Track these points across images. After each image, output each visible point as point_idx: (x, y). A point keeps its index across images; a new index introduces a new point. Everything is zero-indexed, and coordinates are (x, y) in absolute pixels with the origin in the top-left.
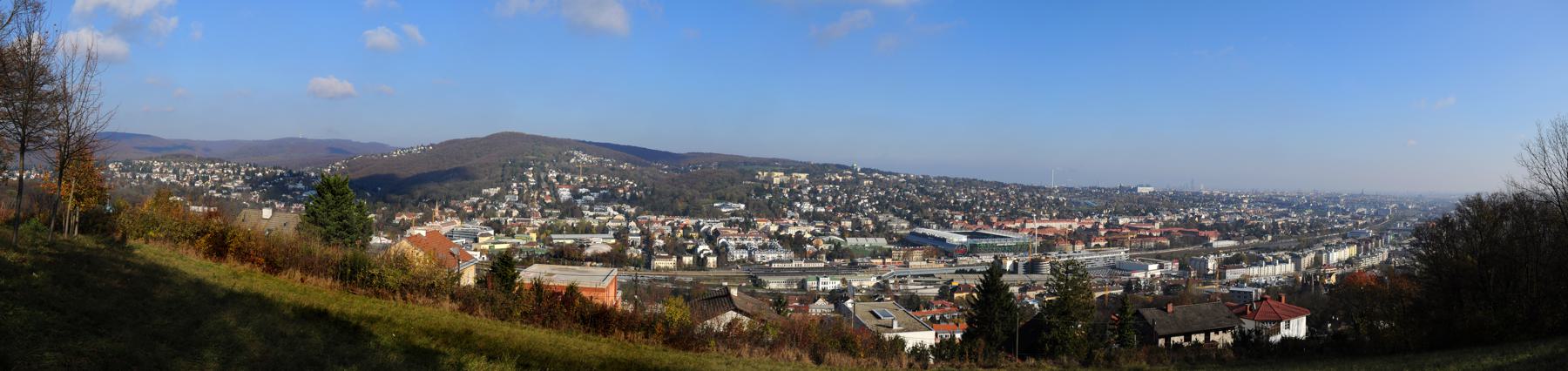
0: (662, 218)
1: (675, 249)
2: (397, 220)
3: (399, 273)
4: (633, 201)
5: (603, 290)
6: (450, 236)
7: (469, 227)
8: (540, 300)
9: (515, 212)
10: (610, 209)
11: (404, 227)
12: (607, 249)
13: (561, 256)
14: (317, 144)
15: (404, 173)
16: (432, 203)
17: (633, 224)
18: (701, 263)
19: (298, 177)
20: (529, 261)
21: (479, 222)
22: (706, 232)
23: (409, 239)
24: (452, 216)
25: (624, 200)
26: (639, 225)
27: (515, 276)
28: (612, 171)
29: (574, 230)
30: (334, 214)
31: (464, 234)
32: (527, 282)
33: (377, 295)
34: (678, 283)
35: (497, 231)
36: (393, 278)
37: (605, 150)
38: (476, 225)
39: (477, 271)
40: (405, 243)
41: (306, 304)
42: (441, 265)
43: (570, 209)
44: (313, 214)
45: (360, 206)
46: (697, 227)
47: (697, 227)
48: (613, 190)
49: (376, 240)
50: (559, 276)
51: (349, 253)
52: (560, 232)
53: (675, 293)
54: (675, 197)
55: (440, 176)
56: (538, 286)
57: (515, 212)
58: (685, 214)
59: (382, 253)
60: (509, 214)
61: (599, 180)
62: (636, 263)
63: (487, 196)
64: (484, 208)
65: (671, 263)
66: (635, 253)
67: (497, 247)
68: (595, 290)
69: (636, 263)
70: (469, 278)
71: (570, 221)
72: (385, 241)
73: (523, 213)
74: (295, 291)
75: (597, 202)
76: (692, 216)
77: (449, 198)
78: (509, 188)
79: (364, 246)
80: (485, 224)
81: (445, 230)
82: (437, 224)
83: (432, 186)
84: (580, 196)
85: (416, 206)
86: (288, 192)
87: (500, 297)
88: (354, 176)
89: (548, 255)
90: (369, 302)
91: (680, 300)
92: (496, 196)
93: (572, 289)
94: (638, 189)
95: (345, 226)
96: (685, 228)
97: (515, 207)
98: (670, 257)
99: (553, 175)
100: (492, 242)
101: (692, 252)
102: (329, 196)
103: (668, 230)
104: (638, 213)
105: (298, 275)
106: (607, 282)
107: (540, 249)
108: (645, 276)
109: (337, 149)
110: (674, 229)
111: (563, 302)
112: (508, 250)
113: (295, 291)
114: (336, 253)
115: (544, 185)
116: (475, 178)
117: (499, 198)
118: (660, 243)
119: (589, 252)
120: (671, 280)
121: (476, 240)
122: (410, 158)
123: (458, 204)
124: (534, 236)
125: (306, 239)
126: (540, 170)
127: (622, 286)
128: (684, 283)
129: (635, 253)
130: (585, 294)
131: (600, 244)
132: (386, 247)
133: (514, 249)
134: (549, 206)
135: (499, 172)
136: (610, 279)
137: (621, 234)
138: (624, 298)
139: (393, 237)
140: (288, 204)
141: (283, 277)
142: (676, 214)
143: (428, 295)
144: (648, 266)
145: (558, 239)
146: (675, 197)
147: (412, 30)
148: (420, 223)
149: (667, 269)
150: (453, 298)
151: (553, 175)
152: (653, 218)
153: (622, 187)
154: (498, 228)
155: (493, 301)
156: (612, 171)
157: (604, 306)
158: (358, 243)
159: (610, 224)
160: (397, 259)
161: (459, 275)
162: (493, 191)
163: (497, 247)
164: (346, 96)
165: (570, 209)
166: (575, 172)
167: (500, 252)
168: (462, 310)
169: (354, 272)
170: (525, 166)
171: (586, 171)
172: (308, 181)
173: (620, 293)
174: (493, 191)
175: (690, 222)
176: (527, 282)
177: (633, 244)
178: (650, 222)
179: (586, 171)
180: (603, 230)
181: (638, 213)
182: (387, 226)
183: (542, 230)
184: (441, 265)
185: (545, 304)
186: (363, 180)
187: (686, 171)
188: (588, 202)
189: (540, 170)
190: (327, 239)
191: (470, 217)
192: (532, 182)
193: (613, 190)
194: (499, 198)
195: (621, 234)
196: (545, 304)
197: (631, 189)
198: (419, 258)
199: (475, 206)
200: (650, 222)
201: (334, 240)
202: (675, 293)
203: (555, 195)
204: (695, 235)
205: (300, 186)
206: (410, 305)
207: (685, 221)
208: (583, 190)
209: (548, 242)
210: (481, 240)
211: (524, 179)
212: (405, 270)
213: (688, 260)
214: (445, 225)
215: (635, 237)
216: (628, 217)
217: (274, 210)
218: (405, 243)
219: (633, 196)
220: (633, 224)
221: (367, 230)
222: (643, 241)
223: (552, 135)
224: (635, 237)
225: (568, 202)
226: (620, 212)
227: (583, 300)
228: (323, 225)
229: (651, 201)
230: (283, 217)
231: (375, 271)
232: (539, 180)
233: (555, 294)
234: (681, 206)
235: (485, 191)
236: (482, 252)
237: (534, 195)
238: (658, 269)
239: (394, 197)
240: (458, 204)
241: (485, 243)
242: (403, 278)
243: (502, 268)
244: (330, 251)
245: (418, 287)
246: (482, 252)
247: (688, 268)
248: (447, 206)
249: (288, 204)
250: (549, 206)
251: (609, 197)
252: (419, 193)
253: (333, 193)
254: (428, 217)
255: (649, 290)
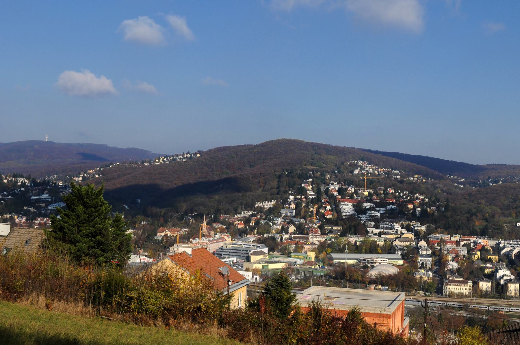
0: (457, 238)
1: (471, 273)
2: (159, 236)
3: (161, 295)
4: (423, 218)
5: (388, 317)
6: (219, 254)
7: (241, 244)
8: (318, 326)
9: (292, 229)
10: (397, 227)
11: (166, 245)
12: (393, 271)
13: (342, 277)
14: (66, 149)
15: (166, 184)
16: (199, 217)
17: (423, 243)
18: (500, 290)
19: (41, 186)
20: (306, 282)
21: (251, 238)
22: (508, 255)
23: (172, 258)
24: (222, 231)
25: (413, 217)
26: (430, 245)
27: (290, 299)
28: (400, 185)
29: (356, 249)
30: (86, 229)
31: (234, 252)
32: (304, 305)
33: (136, 320)
34: (473, 311)
35: (272, 249)
36: (154, 301)
37: (393, 160)
38: (249, 241)
39: (249, 293)
40: (168, 263)
41: (52, 333)
42: (208, 286)
43: (352, 225)
44: (61, 229)
45: (117, 221)
46: (497, 249)
47: (497, 249)
48: (402, 205)
49: (135, 259)
50: (339, 300)
51: (104, 273)
52: (342, 251)
53: (471, 322)
54: (471, 214)
55: (208, 188)
56: (316, 311)
57: (292, 229)
58: (483, 233)
59: (142, 274)
60: (284, 230)
61: (386, 193)
62: (426, 288)
63: (260, 210)
64: (257, 223)
65: (466, 289)
66: (425, 276)
67: (271, 266)
68: (380, 316)
69: (426, 288)
70: (239, 300)
71: (353, 239)
72: (145, 260)
73: (301, 230)
74: (38, 319)
75: (383, 218)
76: (491, 237)
77: (218, 212)
78: (285, 201)
79: (121, 266)
80: (259, 241)
81: (213, 247)
82: (205, 240)
83: (199, 199)
84: (364, 211)
85: (180, 222)
86: (31, 204)
87: (275, 322)
88: (109, 186)
89: (328, 276)
90: (126, 329)
91: (476, 331)
92: (271, 211)
93: (354, 314)
94: (429, 205)
95: (99, 244)
96: (483, 249)
97: (291, 223)
98: (465, 282)
99: (334, 187)
100: (263, 262)
101: (491, 277)
102: (80, 208)
103: (463, 252)
104: (429, 231)
105: (43, 300)
106: (393, 308)
107: (319, 269)
108: (435, 302)
109: (89, 155)
110: (470, 251)
111: (343, 328)
112: (283, 270)
113: (38, 319)
114: (88, 274)
115: (324, 198)
116: (247, 190)
117: (274, 212)
118: (454, 265)
119: (373, 273)
120: (465, 307)
121: (248, 259)
122: (175, 166)
123: (229, 219)
124: (312, 255)
125: (53, 259)
126: (320, 182)
127: (410, 313)
128: (480, 312)
129: (425, 276)
130: (368, 320)
131: (386, 265)
132: (146, 267)
133: (290, 269)
134: (329, 222)
135: (275, 183)
136: (397, 304)
137: (410, 255)
138: (412, 326)
139: (154, 255)
140: (31, 219)
141: (24, 304)
142: (472, 233)
143: (194, 320)
144: (439, 291)
145: (338, 258)
146: (471, 214)
147: (179, 23)
148: (185, 239)
149: (461, 295)
150: (222, 323)
151: (334, 187)
152: (447, 237)
153: (411, 201)
154: (273, 245)
155: (266, 326)
156: (400, 185)
157: (389, 334)
158: (114, 262)
159: (397, 243)
160: (159, 280)
161: (229, 298)
162: (267, 205)
163: (271, 266)
164: (103, 95)
165: (352, 225)
166: (359, 185)
167: (274, 271)
168: (231, 336)
169: (109, 295)
170: (304, 177)
171: (371, 184)
172: (54, 191)
173: (407, 320)
174: (267, 205)
175: (488, 243)
176: (304, 305)
177: (423, 266)
178: (442, 242)
179: (371, 184)
180: (389, 249)
181: (429, 231)
182: (147, 242)
183: (322, 248)
184: (208, 286)
185: (324, 330)
186: (118, 191)
187: (485, 185)
188: (373, 218)
189: (320, 182)
190: (77, 258)
191: (241, 234)
192: (311, 195)
193: (402, 205)
194: (274, 212)
195: (410, 255)
196: (324, 330)
197: (421, 205)
198: (183, 278)
199: (247, 221)
200: (442, 242)
201: (86, 259)
202: (471, 322)
203: (336, 209)
204: (494, 258)
205: (45, 196)
206: (174, 331)
207: (484, 242)
208: (367, 205)
209: (328, 261)
210: (254, 258)
211: (303, 191)
212: (167, 292)
213: (485, 286)
214: (213, 241)
215: (425, 258)
216: (418, 236)
217: (14, 225)
218: (168, 263)
219: (424, 212)
220: (423, 243)
221: (125, 248)
222: (435, 263)
223: (334, 143)
224: (425, 258)
225: (351, 218)
226: (409, 229)
227: (366, 326)
228: (73, 242)
229: (445, 218)
230: (24, 233)
231: (134, 294)
232: (318, 193)
233: (335, 320)
234: (478, 224)
235: (258, 204)
236: (255, 272)
237: (313, 209)
238: (451, 295)
239: (156, 210)
240: (229, 219)
241: (257, 262)
242: (166, 301)
243: (275, 292)
244: (81, 272)
245: (182, 311)
246: (255, 272)
247: (485, 295)
248: (216, 220)
249: (31, 219)
250: (329, 222)
251: (397, 213)
252: (184, 206)
253: (85, 205)
254: (194, 234)
255: (440, 318)
